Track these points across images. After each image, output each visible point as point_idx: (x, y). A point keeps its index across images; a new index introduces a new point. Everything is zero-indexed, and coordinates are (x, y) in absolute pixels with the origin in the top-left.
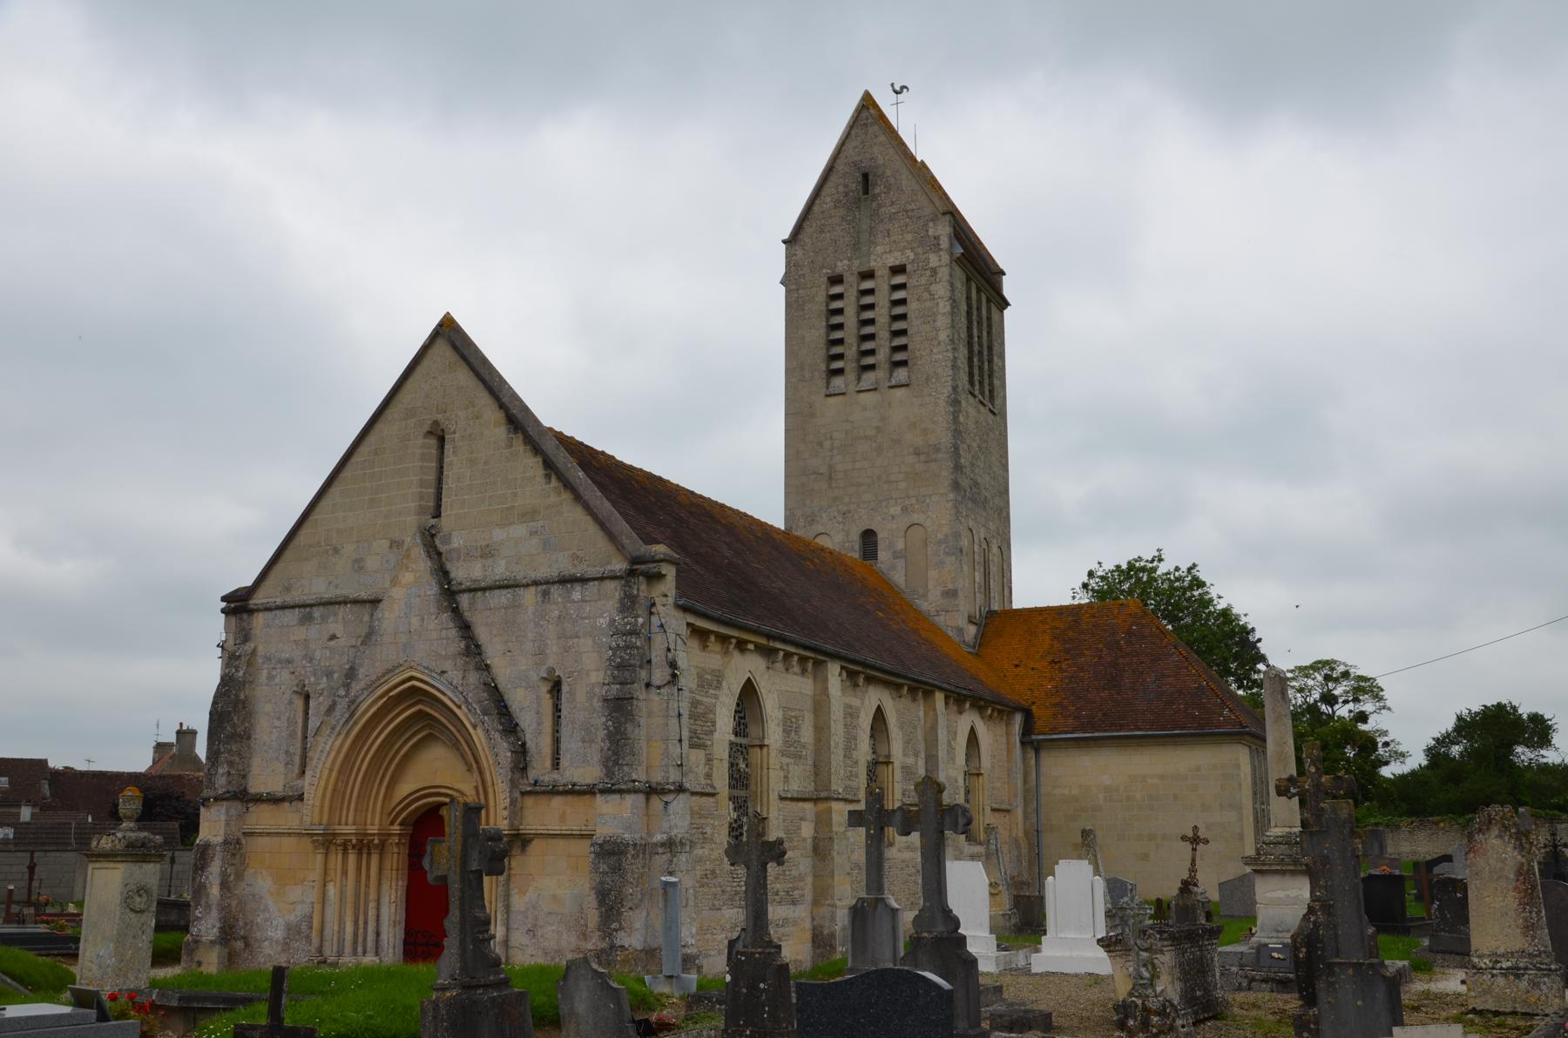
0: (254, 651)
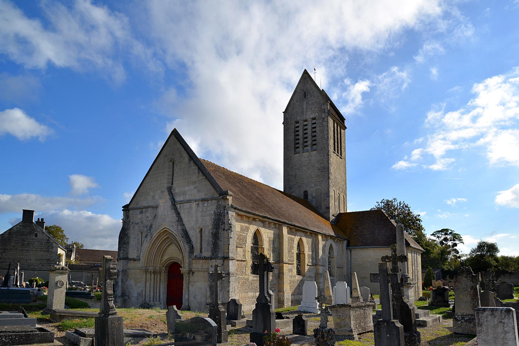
0: (129, 221)
